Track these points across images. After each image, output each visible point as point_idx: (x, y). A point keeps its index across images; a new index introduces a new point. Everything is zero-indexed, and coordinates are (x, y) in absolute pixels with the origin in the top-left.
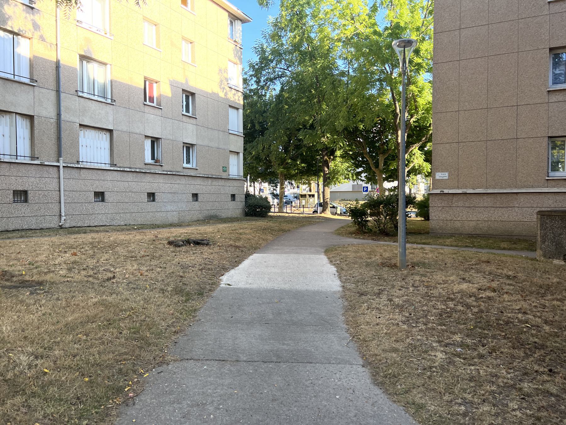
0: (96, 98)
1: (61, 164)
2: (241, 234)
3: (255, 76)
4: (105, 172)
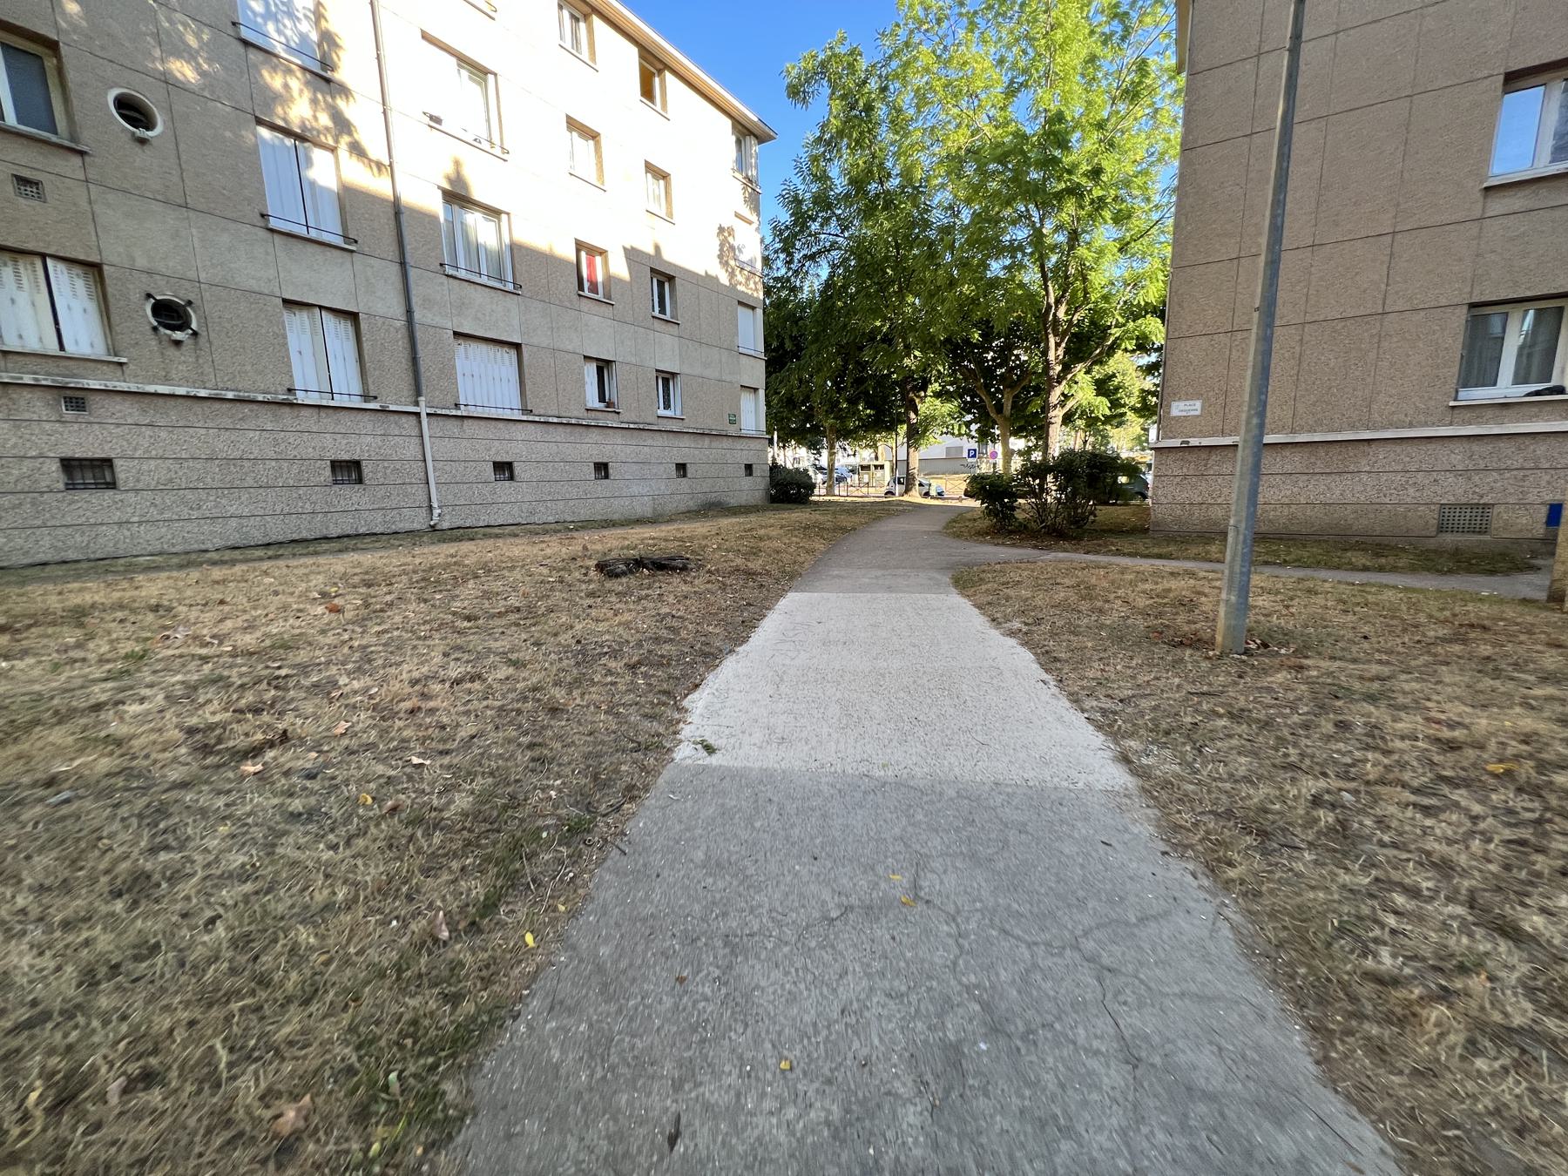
0: (484, 280)
1: (423, 410)
2: (761, 539)
3: (783, 250)
4: (511, 424)
